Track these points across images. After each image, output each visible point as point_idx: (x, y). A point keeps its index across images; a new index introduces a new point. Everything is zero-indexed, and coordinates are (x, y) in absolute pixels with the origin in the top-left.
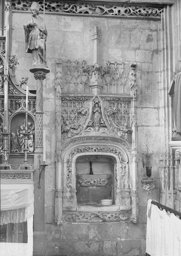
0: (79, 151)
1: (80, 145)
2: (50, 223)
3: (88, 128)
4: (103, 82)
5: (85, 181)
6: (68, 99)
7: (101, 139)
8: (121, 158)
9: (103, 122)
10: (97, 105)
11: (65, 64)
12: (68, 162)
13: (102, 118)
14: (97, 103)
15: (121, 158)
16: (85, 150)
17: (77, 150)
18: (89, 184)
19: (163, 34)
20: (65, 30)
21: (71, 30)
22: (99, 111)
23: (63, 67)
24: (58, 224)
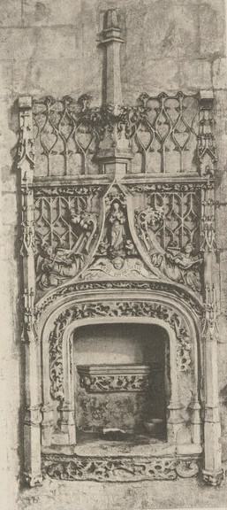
0: (76, 314)
1: (82, 298)
2: (22, 10)
3: (98, 262)
4: (130, 146)
5: (98, 381)
6: (49, 192)
7: (128, 287)
8: (178, 329)
9: (131, 247)
10: (116, 206)
11: (39, 108)
12: (53, 338)
13: (131, 239)
14: (116, 201)
15: (178, 329)
16: (91, 312)
17: (72, 312)
18: (107, 387)
19: (135, 285)
20: (39, 24)
21: (50, 24)
22: (122, 220)
23: (35, 114)
24: (32, 484)
